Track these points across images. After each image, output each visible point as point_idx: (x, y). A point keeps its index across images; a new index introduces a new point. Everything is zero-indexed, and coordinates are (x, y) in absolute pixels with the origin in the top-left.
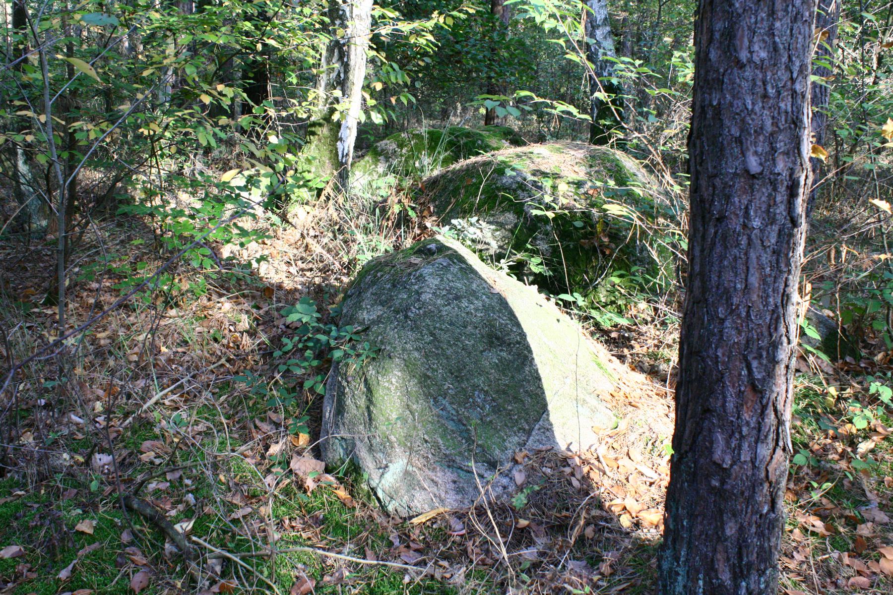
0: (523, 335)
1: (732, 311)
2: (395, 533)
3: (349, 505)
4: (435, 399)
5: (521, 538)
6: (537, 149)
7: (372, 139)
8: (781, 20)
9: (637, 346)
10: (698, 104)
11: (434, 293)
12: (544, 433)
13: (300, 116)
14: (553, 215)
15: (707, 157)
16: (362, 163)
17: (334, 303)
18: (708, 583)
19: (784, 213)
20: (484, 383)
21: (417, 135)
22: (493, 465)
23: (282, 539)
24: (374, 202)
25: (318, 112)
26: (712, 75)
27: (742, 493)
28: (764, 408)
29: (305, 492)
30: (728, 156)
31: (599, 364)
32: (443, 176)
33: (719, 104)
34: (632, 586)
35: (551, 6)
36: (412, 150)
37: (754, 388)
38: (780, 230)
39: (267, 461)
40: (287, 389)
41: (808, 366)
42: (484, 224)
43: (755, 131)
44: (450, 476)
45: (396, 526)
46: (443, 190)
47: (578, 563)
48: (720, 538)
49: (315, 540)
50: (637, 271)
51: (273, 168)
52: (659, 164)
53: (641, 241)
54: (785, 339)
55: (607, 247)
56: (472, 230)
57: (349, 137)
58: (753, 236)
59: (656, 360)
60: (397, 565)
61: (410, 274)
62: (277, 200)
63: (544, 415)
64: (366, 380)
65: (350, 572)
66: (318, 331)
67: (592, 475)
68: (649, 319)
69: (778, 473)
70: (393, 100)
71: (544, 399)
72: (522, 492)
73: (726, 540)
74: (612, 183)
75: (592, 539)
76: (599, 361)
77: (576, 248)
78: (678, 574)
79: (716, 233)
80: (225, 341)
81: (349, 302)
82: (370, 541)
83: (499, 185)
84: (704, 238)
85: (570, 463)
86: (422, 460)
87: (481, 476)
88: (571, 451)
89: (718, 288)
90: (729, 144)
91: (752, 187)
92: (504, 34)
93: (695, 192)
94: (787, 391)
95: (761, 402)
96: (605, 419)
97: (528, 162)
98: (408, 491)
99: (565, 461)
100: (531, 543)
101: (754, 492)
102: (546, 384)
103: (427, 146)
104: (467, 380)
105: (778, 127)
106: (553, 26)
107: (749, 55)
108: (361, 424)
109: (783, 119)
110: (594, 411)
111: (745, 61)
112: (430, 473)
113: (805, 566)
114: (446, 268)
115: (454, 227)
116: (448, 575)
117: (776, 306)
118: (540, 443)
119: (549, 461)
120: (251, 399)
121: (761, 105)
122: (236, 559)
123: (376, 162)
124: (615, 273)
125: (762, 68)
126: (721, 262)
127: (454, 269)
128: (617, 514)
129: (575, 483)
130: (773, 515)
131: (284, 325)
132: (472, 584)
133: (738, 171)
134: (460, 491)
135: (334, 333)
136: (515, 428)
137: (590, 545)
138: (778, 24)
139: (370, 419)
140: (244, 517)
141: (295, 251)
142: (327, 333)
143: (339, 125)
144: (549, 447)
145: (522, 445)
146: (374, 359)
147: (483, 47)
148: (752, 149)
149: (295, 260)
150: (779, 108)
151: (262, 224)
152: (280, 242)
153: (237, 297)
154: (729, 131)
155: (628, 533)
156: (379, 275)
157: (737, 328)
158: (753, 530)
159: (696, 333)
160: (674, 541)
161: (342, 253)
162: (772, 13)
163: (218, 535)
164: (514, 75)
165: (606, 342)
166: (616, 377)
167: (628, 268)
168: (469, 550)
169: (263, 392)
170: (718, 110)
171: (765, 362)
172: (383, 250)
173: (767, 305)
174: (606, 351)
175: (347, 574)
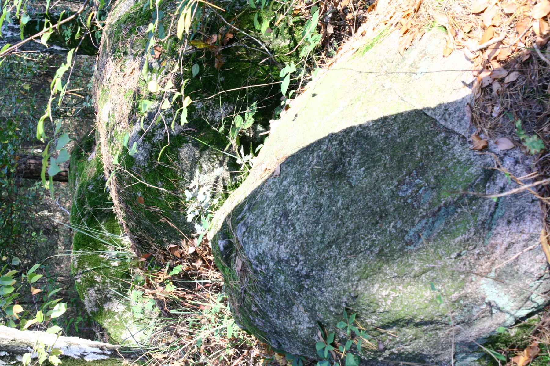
0: (332, 137)
3: (536, 351)
4: (407, 244)
6: (103, 117)
7: (80, 319)
11: (280, 243)
12: (450, 114)
16: (111, 331)
20: (388, 185)
21: (79, 263)
22: (489, 175)
24: (160, 316)
31: (368, 48)
36: (98, 270)
42: (194, 183)
44: (501, 228)
46: (149, 232)
53: (81, 38)
55: (224, 36)
56: (200, 197)
61: (255, 272)
63: (429, 114)
64: (384, 327)
67: (503, 57)
70: (35, 291)
71: (409, 113)
72: (524, 140)
74: (152, 27)
77: (224, 74)
81: (286, 347)
85: (487, 84)
86: (482, 261)
87: (502, 190)
88: (473, 82)
96: (434, 41)
97: (118, 129)
98: (520, 279)
99: (485, 89)
102: (391, 111)
104: (385, 204)
112: (498, 252)
114: (249, 228)
115: (198, 219)
118: (462, 119)
119: (485, 108)
124: (257, 27)
127: (250, 218)
129: (512, 77)
134: (520, 216)
136: (444, 149)
139: (431, 323)
144: (468, 108)
146: (357, 317)
156: (254, 309)
161: (223, 356)
164: (7, 145)
166: (382, 27)
167: (250, 12)
172: (222, 305)
174: (351, 39)
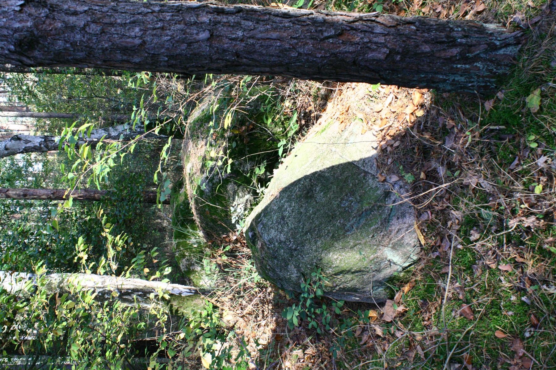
0: (306, 177)
1: (294, 48)
2: (431, 254)
3: (413, 284)
4: (346, 231)
5: (433, 177)
7: (178, 275)
8: (116, 19)
9: (310, 108)
10: (166, 69)
11: (280, 233)
13: (166, 320)
14: (231, 159)
15: (191, 66)
16: (195, 280)
17: (285, 296)
18: (459, 61)
19: (234, 17)
20: (336, 201)
22: (387, 194)
23: (436, 326)
24: (219, 272)
25: (163, 309)
26: (149, 60)
27: (404, 41)
28: (352, 29)
29: (406, 312)
30: (199, 50)
31: (323, 131)
32: (204, 229)
33: (167, 56)
34: (460, 108)
35: (100, 162)
36: (186, 249)
37: (340, 35)
38: (244, 20)
39: (387, 336)
40: (341, 325)
41: (321, 5)
42: (235, 203)
43: (184, 34)
45: (426, 254)
46: (213, 229)
47: (446, 141)
48: (431, 55)
49: (437, 305)
50: (264, 108)
51: (200, 336)
52: (198, 95)
54: (311, 16)
55: (248, 127)
57: (180, 288)
58: (248, 35)
59: (318, 97)
60: (451, 254)
61: (268, 248)
62: (219, 334)
63: (355, 164)
64: (336, 274)
65: (456, 282)
66: (304, 306)
67: (392, 134)
68: (293, 101)
69: (391, 20)
70: (155, 261)
71: (345, 164)
73: (433, 51)
74: (211, 123)
75: (432, 133)
76: (320, 131)
77: (249, 147)
78: (454, 80)
79: (246, 58)
80: (310, 365)
82: (437, 270)
83: (210, 194)
84: (249, 65)
85: (384, 147)
86: (385, 239)
87: (394, 202)
88: (377, 147)
89: (279, 57)
90: (192, 50)
91: (218, 36)
92: (112, 193)
93: (218, 71)
94: (341, 15)
95: (349, 30)
96: (356, 126)
97: (195, 176)
98: (404, 247)
99: (383, 150)
100: (435, 171)
101: (403, 34)
103: (184, 240)
104: (334, 211)
105: (181, 21)
106: (112, 161)
107: (137, 38)
108: (363, 277)
109: (177, 18)
110: (352, 133)
111: (141, 41)
113: (445, 5)
114: (264, 225)
115: (237, 222)
116: (457, 221)
117: (290, 21)
119: (384, 160)
120: (347, 347)
121: (168, 31)
122: (451, 354)
123: (194, 271)
124: (265, 122)
125: (145, 30)
126: (263, 55)
127: (265, 220)
128: (416, 118)
129: (397, 144)
130: (417, 23)
131: (299, 327)
132: (462, 206)
133: (208, 45)
135: (306, 295)
137: (435, 134)
138: (119, 21)
140: (423, 350)
141: (251, 322)
142: (305, 299)
143: (171, 295)
144: (375, 161)
145: (374, 177)
146: (322, 270)
147: (121, 206)
148: (195, 36)
149: (257, 322)
150: (169, 20)
151: (234, 343)
152: (245, 331)
153: (282, 358)
154: (184, 50)
155: (427, 111)
156: (268, 267)
157: (304, 45)
158: (426, 35)
159: (307, 70)
160: (434, 82)
161: (252, 292)
162: (112, 24)
163: (435, 366)
164: (138, 186)
165: (308, 126)
166: (330, 120)
167: (262, 114)
168: (441, 208)
169: (343, 340)
170: (171, 57)
171: (324, 28)
172: (251, 266)
173: (289, 27)
174: (314, 126)
175: (458, 284)
